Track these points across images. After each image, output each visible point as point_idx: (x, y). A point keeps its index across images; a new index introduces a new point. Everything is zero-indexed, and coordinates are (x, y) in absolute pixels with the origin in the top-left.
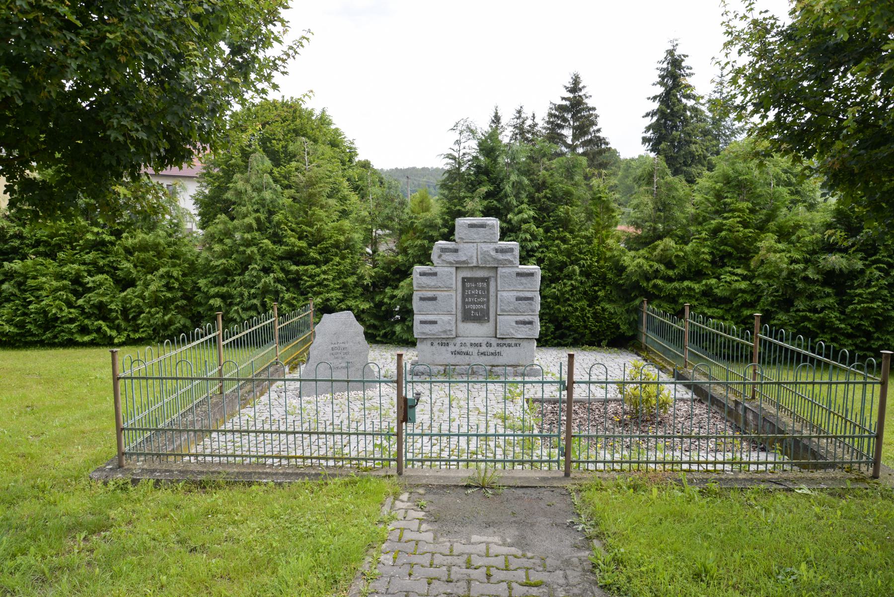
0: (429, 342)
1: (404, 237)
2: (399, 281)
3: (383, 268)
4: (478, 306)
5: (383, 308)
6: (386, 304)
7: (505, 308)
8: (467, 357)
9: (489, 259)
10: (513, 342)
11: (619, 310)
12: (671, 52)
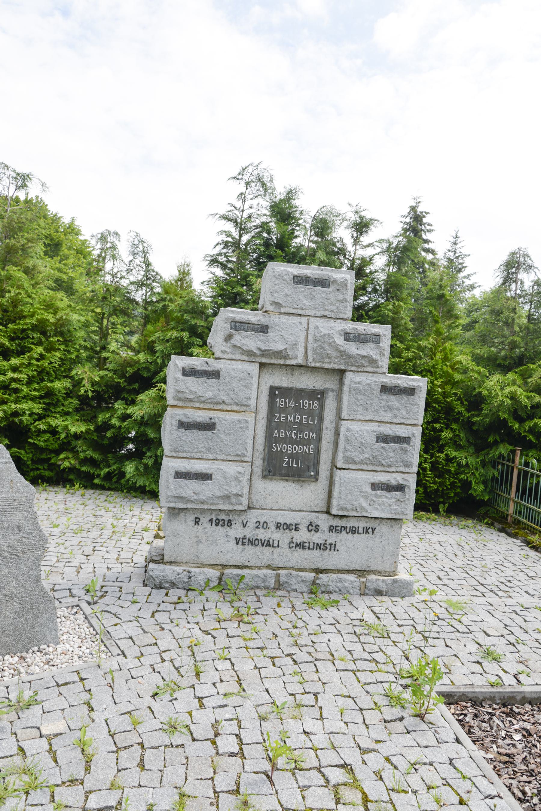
0: (191, 518)
1: (149, 327)
2: (138, 392)
3: (115, 372)
4: (298, 449)
5: (109, 434)
6: (113, 426)
7: (354, 455)
8: (267, 551)
9: (331, 352)
10: (362, 524)
11: (472, 461)
12: (413, 209)
